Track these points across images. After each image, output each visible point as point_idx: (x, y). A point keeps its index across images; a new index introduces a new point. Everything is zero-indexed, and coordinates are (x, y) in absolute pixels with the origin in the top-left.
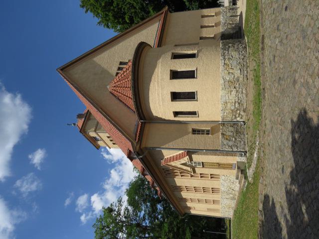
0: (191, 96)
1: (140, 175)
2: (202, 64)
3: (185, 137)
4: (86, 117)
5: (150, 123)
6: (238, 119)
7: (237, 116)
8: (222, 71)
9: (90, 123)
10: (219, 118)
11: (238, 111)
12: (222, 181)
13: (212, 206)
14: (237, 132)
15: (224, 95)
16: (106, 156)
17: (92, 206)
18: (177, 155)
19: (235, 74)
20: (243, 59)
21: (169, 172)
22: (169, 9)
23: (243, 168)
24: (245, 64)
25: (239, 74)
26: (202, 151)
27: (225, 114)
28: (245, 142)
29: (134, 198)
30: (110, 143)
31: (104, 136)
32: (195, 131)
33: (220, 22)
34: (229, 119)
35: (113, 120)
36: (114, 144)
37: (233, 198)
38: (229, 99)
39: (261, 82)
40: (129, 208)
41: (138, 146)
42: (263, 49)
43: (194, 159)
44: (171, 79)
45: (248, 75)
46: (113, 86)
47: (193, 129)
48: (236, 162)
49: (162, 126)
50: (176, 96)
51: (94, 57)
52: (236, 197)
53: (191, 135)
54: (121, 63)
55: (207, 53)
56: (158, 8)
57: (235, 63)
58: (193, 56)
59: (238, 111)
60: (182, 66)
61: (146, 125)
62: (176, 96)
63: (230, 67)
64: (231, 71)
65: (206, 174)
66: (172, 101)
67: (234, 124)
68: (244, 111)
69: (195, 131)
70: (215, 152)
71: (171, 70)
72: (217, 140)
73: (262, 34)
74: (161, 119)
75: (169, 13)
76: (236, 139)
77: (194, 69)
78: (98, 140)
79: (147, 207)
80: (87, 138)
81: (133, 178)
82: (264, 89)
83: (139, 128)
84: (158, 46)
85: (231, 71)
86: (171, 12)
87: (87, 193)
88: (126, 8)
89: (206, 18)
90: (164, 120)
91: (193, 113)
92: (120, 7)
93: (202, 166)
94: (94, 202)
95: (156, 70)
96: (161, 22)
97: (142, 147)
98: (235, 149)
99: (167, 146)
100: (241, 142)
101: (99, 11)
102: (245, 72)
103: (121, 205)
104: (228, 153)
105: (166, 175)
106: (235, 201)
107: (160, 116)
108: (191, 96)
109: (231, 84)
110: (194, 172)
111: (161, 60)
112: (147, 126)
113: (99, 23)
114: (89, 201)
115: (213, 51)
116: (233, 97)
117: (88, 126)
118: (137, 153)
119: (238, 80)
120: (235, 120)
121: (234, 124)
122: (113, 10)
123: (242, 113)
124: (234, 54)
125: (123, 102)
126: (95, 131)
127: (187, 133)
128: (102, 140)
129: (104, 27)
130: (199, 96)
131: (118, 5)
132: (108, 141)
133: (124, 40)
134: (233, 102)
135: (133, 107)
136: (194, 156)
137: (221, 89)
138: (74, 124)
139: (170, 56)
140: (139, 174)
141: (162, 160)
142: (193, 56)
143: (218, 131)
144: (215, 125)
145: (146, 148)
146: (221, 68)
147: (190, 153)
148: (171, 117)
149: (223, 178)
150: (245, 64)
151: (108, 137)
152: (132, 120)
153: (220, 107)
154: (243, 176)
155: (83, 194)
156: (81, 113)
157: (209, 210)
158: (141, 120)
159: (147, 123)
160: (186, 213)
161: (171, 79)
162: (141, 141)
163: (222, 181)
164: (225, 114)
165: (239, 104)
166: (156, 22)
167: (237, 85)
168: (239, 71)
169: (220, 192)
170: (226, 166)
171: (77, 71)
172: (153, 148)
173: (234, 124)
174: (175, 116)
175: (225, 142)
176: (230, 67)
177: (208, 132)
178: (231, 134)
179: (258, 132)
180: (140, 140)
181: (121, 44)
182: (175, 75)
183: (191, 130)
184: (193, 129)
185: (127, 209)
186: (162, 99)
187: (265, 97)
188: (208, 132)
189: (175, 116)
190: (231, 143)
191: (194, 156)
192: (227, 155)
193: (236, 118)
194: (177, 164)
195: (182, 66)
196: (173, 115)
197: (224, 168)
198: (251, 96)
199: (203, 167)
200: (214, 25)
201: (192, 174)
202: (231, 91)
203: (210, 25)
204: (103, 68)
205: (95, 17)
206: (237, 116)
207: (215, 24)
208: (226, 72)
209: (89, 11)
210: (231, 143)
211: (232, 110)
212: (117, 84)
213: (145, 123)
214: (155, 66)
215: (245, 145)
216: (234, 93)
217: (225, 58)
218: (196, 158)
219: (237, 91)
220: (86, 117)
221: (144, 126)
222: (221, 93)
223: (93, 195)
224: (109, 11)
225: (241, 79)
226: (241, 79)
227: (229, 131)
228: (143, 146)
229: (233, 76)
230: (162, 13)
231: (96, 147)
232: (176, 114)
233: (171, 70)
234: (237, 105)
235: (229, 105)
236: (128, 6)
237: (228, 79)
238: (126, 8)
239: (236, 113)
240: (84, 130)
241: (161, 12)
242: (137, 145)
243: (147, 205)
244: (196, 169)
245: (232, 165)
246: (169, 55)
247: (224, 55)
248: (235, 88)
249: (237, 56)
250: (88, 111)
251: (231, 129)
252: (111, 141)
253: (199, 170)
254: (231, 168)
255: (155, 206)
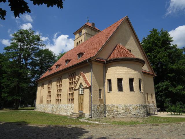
0: (120, 88)
1: (56, 57)
2: (137, 94)
3: (97, 85)
4: (93, 28)
5: (104, 66)
6: (107, 114)
7: (109, 113)
8: (134, 105)
9: (90, 30)
10: (107, 103)
11: (112, 114)
12: (67, 105)
13: (45, 99)
14: (101, 113)
15: (122, 106)
16: (55, 35)
17: (24, 24)
18: (88, 82)
19: (132, 112)
20: (140, 115)
21: (72, 75)
22: (155, 77)
23: (82, 116)
24: (138, 117)
25: (133, 114)
26: (91, 94)
27: (111, 107)
28: (96, 117)
29: (43, 53)
30: (77, 41)
31: (83, 38)
32: (100, 90)
33: (150, 103)
34: (107, 109)
35: (105, 46)
36: (77, 43)
37: (53, 111)
38: (119, 109)
39: (137, 125)
40: (38, 50)
41: (94, 60)
42: (153, 125)
43: (85, 90)
44: (129, 78)
45: (133, 118)
46: (122, 47)
47: (101, 89)
48: (84, 112)
49: (102, 73)
50: (120, 80)
51: (133, 36)
52: (54, 113)
53: (98, 88)
54: (130, 51)
55: (142, 97)
56: (155, 70)
57: (138, 111)
58: (140, 90)
59: (112, 114)
60: (126, 84)
61: (103, 64)
62: (120, 80)
63: (136, 109)
64: (134, 109)
65: (51, 94)
66: (117, 79)
67: (104, 111)
68: (113, 117)
69: (100, 90)
70: (91, 101)
71: (133, 78)
72: (97, 103)
73: (159, 124)
74: (106, 72)
75: (153, 77)
76: (97, 112)
77: (134, 91)
78: (79, 34)
79: (37, 61)
80: (81, 27)
81: (54, 53)
82: (135, 126)
83: (101, 60)
84: (143, 72)
85: (134, 109)
86: (153, 78)
87: (33, 21)
88: (154, 54)
89: (151, 96)
90: (106, 74)
91: (110, 89)
92: (155, 50)
93: (79, 94)
94: (27, 25)
95: (133, 71)
96: (149, 72)
97: (93, 62)
98: (93, 112)
99: (93, 75)
100: (96, 115)
101: (152, 39)
102: (134, 117)
103: (40, 46)
104: (90, 108)
105: (70, 74)
106: (50, 112)
107: (108, 72)
108: (120, 88)
109: (128, 109)
110: (75, 90)
111: (138, 73)
112: (102, 65)
113: (144, 38)
114: (29, 22)
115: (143, 100)
116: (121, 110)
117: (88, 29)
118: (90, 59)
119: (130, 113)
120: (106, 112)
121: (104, 111)
122: (152, 47)
123: (111, 116)
124: (142, 111)
125: (113, 52)
126: (86, 33)
127: (99, 86)
128: (80, 37)
129: (142, 41)
130: (120, 93)
131: (156, 49)
132: (80, 39)
133: (141, 52)
134: (118, 110)
135: (110, 59)
136: (88, 90)
137: (125, 104)
138: (88, 21)
139: (140, 78)
140: (57, 56)
141: (83, 72)
142: (140, 90)
143: (100, 103)
144: (104, 101)
145: (92, 64)
146: (136, 105)
147: (90, 88)
148: (108, 77)
149: (70, 106)
150: (138, 117)
151: (82, 40)
152: (104, 57)
153: (114, 104)
154: (78, 116)
155: (32, 18)
156: (95, 25)
157: (42, 97)
158: (106, 62)
159: (104, 65)
160: (38, 84)
161: (129, 78)
162: (95, 61)
163: (67, 105)
164: (111, 107)
165: (117, 114)
166: (149, 69)
167: (127, 113)
168: (134, 114)
169: (57, 104)
170: (81, 107)
171: (126, 27)
172: (92, 68)
173: (104, 111)
174: (108, 80)
175: (96, 107)
176: (136, 109)
177: (100, 97)
178: (100, 109)
179: (110, 124)
180: (97, 61)
181: (139, 51)
182: (131, 80)
183: (101, 88)
184: (101, 89)
185: (38, 49)
186: (119, 73)
187: (132, 126)
188: (100, 97)
189: (108, 80)
190: (95, 110)
191: (88, 90)
192: (89, 108)
193: (108, 112)
194: (81, 80)
195: (136, 84)
196: (109, 78)
197: (79, 106)
198: (122, 120)
199: (79, 95)
200: (148, 100)
201: (74, 89)
202: (124, 110)
203: (148, 98)
204: (128, 41)
205: (147, 36)
206: (109, 113)
207: (149, 101)
208: (134, 107)
209: (151, 33)
210: (95, 110)
211: (113, 110)
212: (123, 49)
213: (104, 64)
214: (135, 70)
215: (95, 117)
216: (123, 111)
217: (140, 106)
218: (87, 92)
219: (124, 113)
220: (93, 28)
221: (102, 63)
222: (123, 105)
223: (32, 24)
224: (152, 44)
225: (130, 115)
226: (130, 115)
227: (102, 109)
228: (93, 63)
229: (132, 110)
230: (153, 73)
231: (75, 33)
232: (110, 81)
233: (133, 78)
234: (116, 113)
235: (116, 109)
236: (155, 55)
237: (130, 108)
238: (154, 54)
239: (112, 112)
240: (87, 27)
241: (154, 72)
242: (94, 59)
243: (38, 61)
244: (78, 91)
245: (81, 110)
246: (141, 78)
247: (141, 106)
248: (126, 112)
249: (141, 113)
250: (100, 31)
251: (102, 110)
252: (79, 42)
253: (77, 93)
254: (79, 110)
255: (39, 66)
